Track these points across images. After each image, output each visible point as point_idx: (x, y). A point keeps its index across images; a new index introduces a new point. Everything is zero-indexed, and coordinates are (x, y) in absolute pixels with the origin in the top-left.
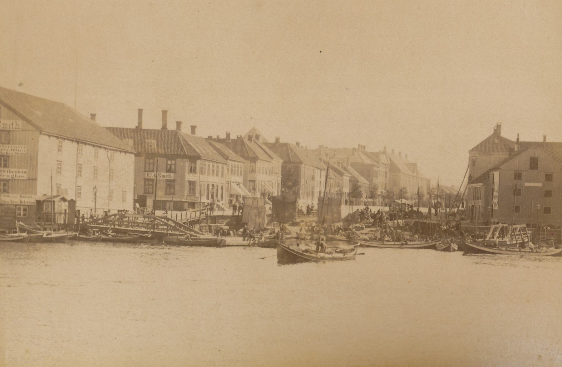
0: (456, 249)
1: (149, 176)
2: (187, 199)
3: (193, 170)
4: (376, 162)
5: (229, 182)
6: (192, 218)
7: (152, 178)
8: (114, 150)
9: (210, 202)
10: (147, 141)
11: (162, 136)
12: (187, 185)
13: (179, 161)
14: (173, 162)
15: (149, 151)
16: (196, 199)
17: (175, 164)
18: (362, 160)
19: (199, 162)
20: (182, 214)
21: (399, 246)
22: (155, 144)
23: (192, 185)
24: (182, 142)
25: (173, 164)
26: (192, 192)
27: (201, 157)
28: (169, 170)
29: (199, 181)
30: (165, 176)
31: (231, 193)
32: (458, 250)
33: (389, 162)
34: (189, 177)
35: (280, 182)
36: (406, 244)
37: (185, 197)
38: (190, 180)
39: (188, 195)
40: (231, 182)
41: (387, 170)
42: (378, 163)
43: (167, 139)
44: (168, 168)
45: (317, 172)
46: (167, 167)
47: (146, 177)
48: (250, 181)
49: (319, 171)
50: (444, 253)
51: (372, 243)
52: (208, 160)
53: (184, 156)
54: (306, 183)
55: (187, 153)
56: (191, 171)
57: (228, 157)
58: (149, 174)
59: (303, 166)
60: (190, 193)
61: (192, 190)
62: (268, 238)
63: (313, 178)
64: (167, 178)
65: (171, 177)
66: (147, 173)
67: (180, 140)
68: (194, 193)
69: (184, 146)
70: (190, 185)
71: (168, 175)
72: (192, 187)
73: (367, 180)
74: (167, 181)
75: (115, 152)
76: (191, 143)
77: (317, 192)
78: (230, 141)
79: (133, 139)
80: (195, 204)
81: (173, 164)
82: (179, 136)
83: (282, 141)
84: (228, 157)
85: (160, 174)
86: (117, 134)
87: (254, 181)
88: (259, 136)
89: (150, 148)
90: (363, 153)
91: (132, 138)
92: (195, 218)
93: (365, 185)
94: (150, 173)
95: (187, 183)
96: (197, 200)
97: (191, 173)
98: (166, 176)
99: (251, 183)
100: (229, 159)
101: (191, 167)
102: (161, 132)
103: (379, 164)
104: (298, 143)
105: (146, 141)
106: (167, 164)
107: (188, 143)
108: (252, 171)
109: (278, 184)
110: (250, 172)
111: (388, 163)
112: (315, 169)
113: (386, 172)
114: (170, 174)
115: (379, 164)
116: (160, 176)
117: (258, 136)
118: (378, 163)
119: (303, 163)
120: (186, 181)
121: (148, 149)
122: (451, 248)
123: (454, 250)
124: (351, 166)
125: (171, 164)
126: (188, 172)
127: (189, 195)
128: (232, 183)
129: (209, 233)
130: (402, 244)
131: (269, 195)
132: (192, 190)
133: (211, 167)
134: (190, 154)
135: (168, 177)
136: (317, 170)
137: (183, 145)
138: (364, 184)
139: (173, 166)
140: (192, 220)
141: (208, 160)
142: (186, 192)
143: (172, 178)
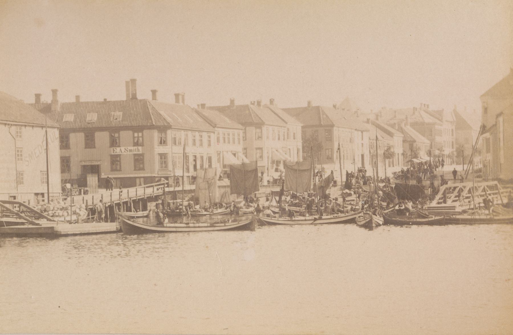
0: (381, 223)
1: (115, 152)
2: (159, 173)
3: (163, 142)
4: (438, 119)
5: (220, 152)
6: (138, 195)
7: (118, 154)
8: (22, 125)
9: (191, 175)
10: (113, 113)
11: (138, 108)
12: (157, 158)
13: (146, 132)
14: (140, 134)
15: (114, 124)
16: (169, 173)
17: (142, 137)
18: (423, 118)
19: (169, 132)
20: (128, 190)
21: (311, 222)
22: (121, 116)
23: (163, 158)
24: (150, 112)
25: (141, 137)
26: (164, 165)
27: (171, 126)
28: (136, 144)
29: (172, 153)
30: (133, 150)
31: (225, 163)
32: (384, 224)
33: (455, 120)
34: (160, 149)
35: (301, 148)
36: (320, 218)
37: (156, 173)
38: (160, 152)
39: (159, 170)
40: (223, 152)
41: (454, 127)
42: (441, 120)
43: (134, 109)
44: (136, 141)
45: (357, 135)
46: (134, 141)
47: (113, 154)
48: (257, 149)
49: (360, 133)
50: (363, 230)
51: (271, 219)
52: (183, 129)
53: (152, 127)
54: (342, 147)
55: (154, 123)
56: (161, 143)
57: (216, 125)
58: (115, 149)
59: (335, 128)
60: (162, 167)
61: (163, 163)
62: (220, 214)
63: (351, 141)
64: (135, 153)
65: (139, 150)
66: (113, 149)
67: (148, 109)
68: (166, 167)
69: (152, 116)
70: (161, 158)
71: (136, 149)
72: (163, 160)
73: (428, 139)
74: (135, 155)
75: (23, 128)
76: (162, 113)
77: (359, 155)
78: (235, 107)
79: (98, 113)
80: (168, 178)
81: (141, 137)
82: (149, 106)
83: (314, 104)
84: (216, 125)
85: (127, 148)
86: (81, 108)
87: (261, 149)
88: (274, 100)
89: (114, 121)
90: (424, 111)
91: (96, 113)
92: (144, 196)
93: (425, 144)
94: (116, 149)
95: (158, 155)
96: (171, 174)
97: (161, 145)
98: (134, 150)
99: (258, 151)
100: (217, 126)
101: (161, 138)
102: (129, 103)
103: (442, 122)
104: (335, 105)
105: (111, 114)
106: (134, 137)
107: (158, 112)
108: (258, 138)
109: (298, 150)
110: (256, 140)
111: (454, 120)
112: (353, 131)
113: (452, 130)
114: (138, 148)
115: (442, 122)
116: (128, 151)
117: (272, 100)
118: (441, 120)
119: (335, 126)
120: (156, 154)
121: (113, 122)
122: (373, 221)
123: (378, 225)
124: (411, 126)
125: (138, 137)
126: (157, 145)
127: (160, 169)
128: (225, 153)
129: (330, 198)
130: (315, 219)
131: (284, 162)
132: (163, 163)
133: (236, 135)
134: (158, 124)
135: (136, 151)
136: (356, 132)
137: (151, 114)
138: (424, 143)
139: (141, 139)
140: (138, 198)
141: (183, 129)
142: (157, 166)
143: (141, 152)
